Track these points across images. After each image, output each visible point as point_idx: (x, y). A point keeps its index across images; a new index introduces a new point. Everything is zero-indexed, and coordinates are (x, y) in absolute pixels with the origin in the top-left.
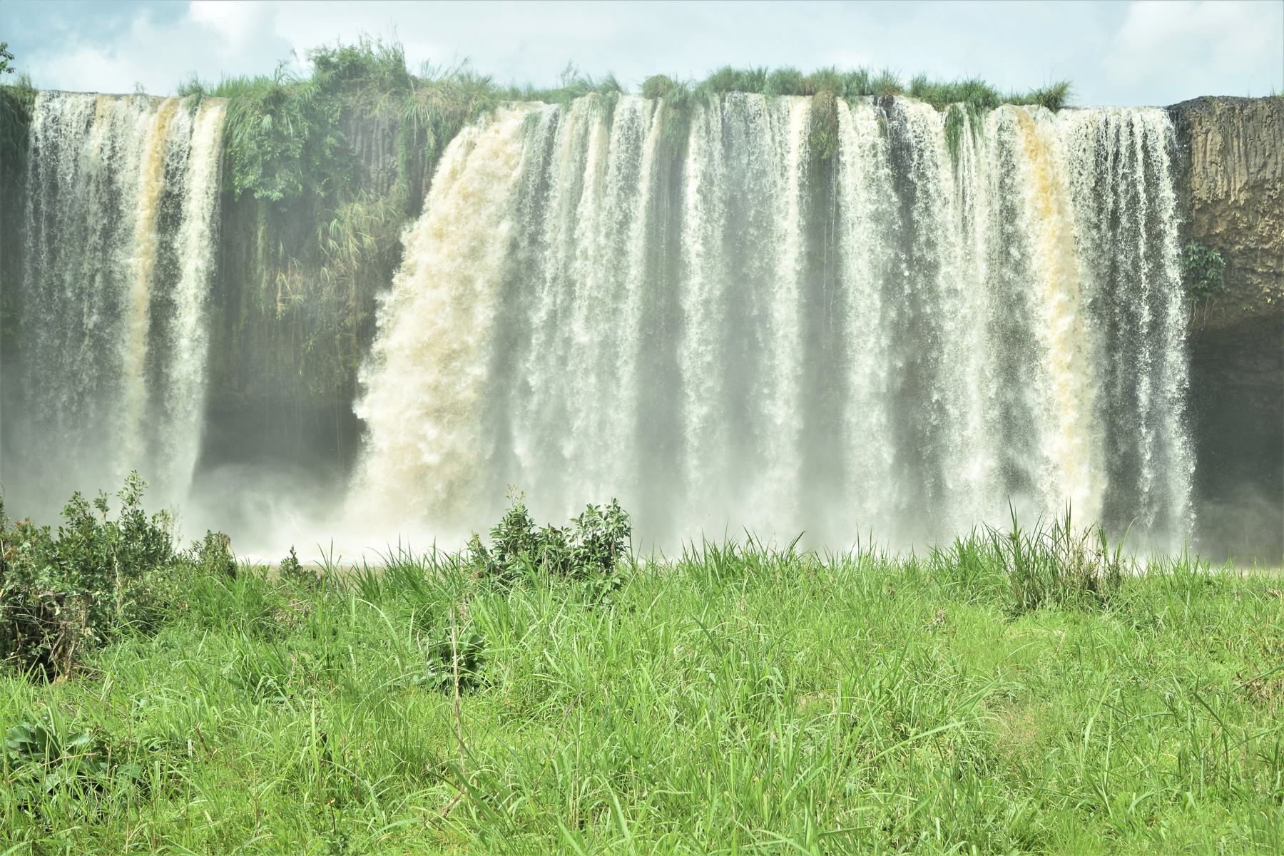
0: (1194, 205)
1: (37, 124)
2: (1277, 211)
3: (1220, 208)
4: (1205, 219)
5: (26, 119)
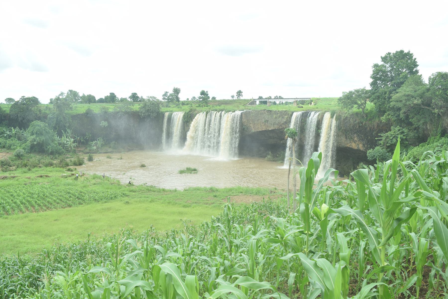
5: (172, 115)
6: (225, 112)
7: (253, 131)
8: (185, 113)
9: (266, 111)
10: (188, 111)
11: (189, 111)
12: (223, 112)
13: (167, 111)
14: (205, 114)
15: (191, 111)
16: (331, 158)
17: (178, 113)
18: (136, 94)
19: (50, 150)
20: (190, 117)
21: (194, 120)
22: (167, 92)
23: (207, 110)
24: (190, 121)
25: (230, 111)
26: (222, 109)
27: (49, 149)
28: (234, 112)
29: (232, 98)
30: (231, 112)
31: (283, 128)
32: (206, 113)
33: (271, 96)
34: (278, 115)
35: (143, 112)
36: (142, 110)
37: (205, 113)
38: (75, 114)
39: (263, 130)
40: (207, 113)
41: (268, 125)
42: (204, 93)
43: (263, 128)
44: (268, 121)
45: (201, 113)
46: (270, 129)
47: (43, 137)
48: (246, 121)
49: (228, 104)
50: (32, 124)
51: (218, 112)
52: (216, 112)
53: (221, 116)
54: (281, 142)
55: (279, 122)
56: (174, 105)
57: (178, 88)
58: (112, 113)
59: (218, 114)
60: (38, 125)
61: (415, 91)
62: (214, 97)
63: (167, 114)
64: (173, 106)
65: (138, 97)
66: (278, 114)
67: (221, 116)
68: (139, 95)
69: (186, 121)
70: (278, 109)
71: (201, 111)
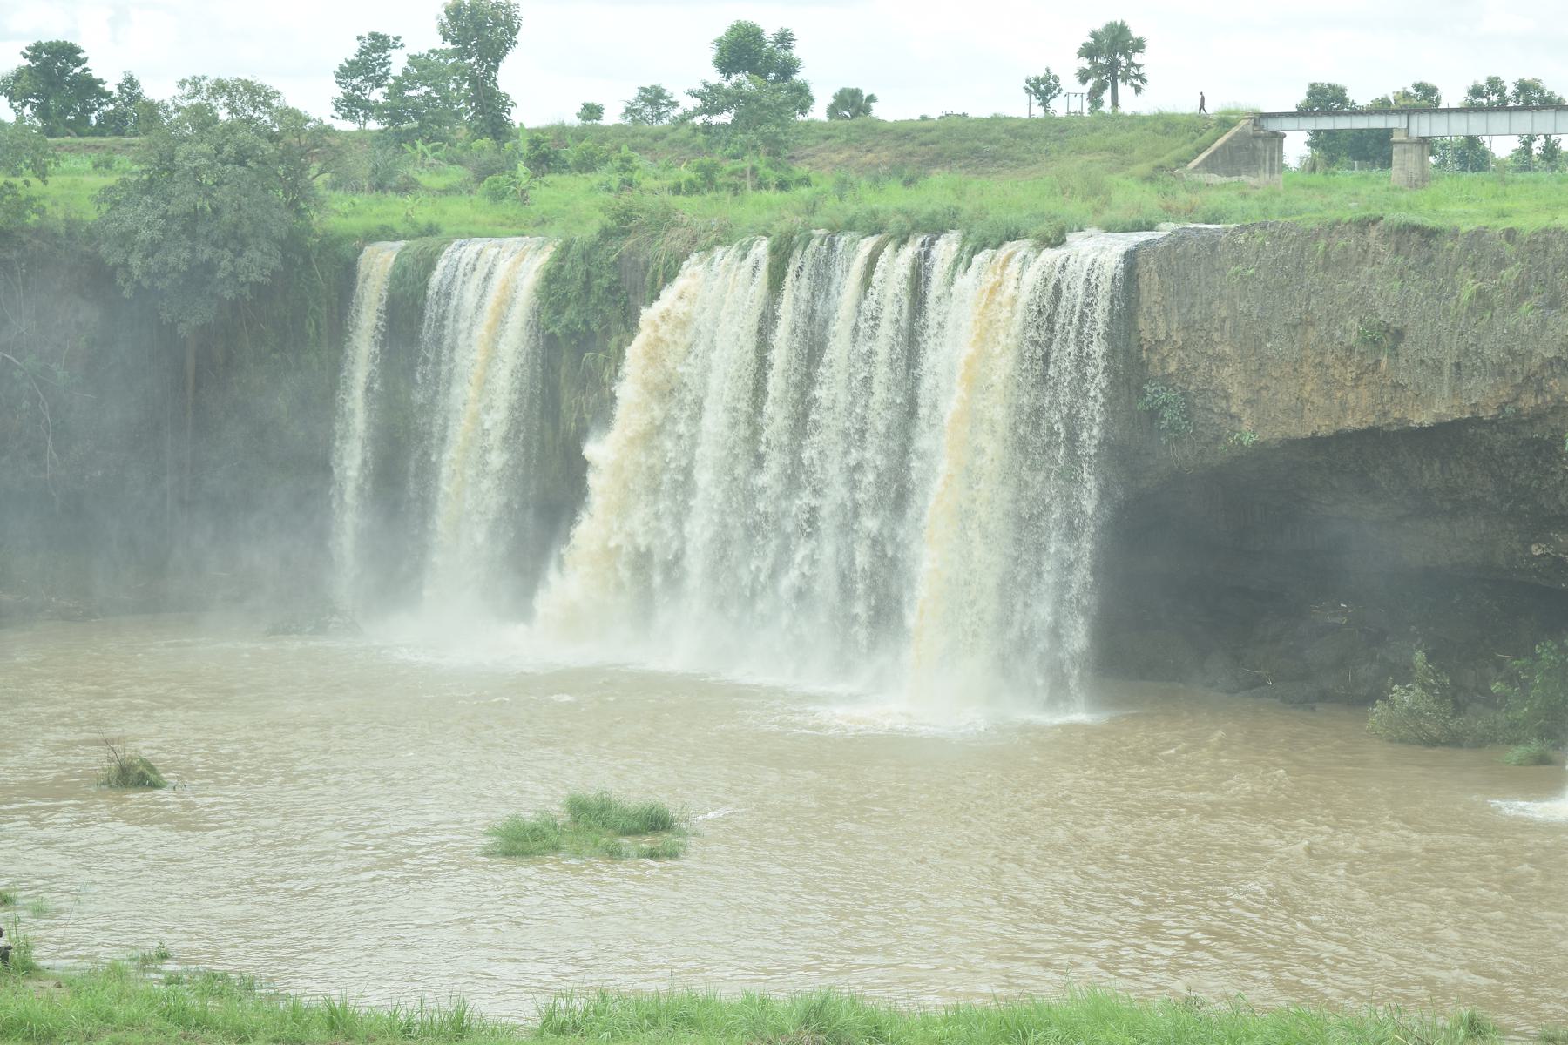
0: (1142, 346)
1: (436, 278)
2: (1210, 352)
3: (1165, 349)
4: (1155, 358)
5: (430, 266)
6: (965, 239)
7: (1248, 439)
8: (566, 248)
9: (1385, 238)
11: (606, 234)
12: (946, 248)
13: (385, 233)
15: (626, 233)
18: (69, 52)
20: (613, 289)
23: (781, 227)
24: (607, 333)
25: (1013, 235)
26: (932, 218)
29: (1035, 102)
30: (1021, 247)
31: (1554, 411)
32: (774, 251)
33: (1430, 81)
34: (1510, 274)
39: (1351, 423)
41: (1403, 377)
42: (758, 54)
43: (1344, 407)
44: (1399, 335)
46: (1423, 418)
48: (1178, 337)
49: (995, 159)
51: (889, 250)
52: (867, 245)
53: (918, 280)
54: (1536, 550)
55: (1517, 346)
56: (456, 175)
59: (897, 265)
62: (856, 93)
63: (378, 263)
64: (439, 182)
65: (89, 87)
66: (1501, 263)
67: (918, 280)
68: (106, 68)
71: (725, 235)
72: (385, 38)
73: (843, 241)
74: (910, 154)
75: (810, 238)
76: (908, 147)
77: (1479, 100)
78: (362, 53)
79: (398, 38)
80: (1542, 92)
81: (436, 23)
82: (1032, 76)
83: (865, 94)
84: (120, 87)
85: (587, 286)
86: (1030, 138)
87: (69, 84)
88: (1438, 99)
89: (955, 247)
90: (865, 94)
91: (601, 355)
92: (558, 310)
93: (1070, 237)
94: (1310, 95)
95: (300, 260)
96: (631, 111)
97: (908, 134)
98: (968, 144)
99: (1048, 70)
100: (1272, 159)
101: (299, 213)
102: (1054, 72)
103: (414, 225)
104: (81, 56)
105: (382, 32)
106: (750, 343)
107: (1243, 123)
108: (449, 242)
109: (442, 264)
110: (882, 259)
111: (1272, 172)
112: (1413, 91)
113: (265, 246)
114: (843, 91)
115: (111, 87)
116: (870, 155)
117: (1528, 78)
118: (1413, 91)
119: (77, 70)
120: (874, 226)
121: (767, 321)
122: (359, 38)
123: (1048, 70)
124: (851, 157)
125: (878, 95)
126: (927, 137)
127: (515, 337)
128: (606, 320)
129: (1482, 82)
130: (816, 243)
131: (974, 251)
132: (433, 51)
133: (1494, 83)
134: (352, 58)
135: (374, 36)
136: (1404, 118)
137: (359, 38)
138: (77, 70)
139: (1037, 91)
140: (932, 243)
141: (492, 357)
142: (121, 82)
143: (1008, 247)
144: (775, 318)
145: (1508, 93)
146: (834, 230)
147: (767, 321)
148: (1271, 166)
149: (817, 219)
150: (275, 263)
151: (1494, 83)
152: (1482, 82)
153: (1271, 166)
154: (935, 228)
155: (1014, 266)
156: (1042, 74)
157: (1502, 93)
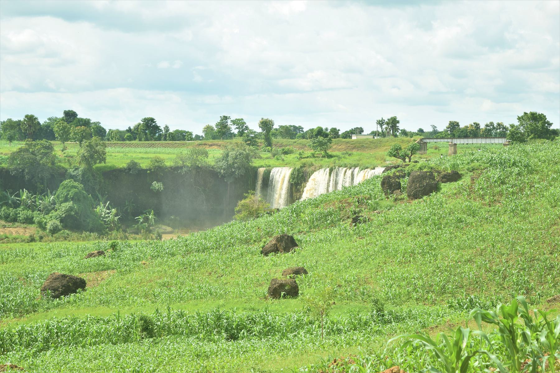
1: (271, 174)
5: (270, 172)
6: (360, 168)
8: (295, 169)
10: (298, 167)
11: (301, 167)
12: (357, 169)
13: (262, 166)
14: (328, 171)
15: (304, 167)
16: (381, 185)
17: (280, 169)
18: (152, 120)
19: (91, 225)
20: (302, 176)
21: (310, 180)
22: (226, 118)
23: (331, 166)
24: (301, 183)
25: (367, 168)
26: (355, 165)
27: (89, 223)
28: (374, 169)
29: (379, 126)
30: (369, 170)
32: (330, 170)
33: (478, 122)
35: (224, 167)
36: (221, 164)
37: (328, 170)
38: (109, 170)
40: (331, 171)
42: (322, 132)
45: (322, 171)
47: (81, 204)
49: (367, 147)
50: (63, 185)
51: (348, 169)
52: (345, 169)
53: (353, 175)
56: (269, 155)
57: (270, 119)
58: (170, 169)
59: (349, 172)
60: (75, 186)
61: (26, 228)
62: (335, 129)
63: (262, 170)
64: (265, 156)
65: (157, 128)
67: (353, 175)
68: (161, 123)
69: (295, 183)
70: (22, 245)
71: (321, 167)
72: (227, 117)
73: (340, 169)
74: (349, 146)
75: (335, 168)
76: (348, 145)
77: (488, 127)
78: (221, 120)
79: (230, 117)
80: (503, 126)
81: (258, 125)
82: (378, 120)
83: (337, 129)
84: (164, 128)
85: (298, 176)
86: (374, 143)
87: (152, 127)
88: (480, 126)
89: (358, 169)
90: (337, 129)
91: (300, 187)
92: (293, 179)
93: (375, 168)
94: (449, 124)
95: (248, 171)
96: (359, 184)
97: (348, 142)
98: (361, 144)
99: (382, 118)
100: (425, 148)
101: (248, 163)
102: (384, 119)
103: (266, 165)
104: (155, 121)
105: (226, 116)
106: (326, 185)
107: (418, 140)
108: (273, 168)
109: (272, 172)
110: (347, 171)
111: (424, 150)
112: (473, 124)
113: (243, 169)
114: (332, 128)
115: (162, 128)
116: (340, 147)
117: (500, 122)
118: (473, 124)
119: (154, 124)
120: (346, 166)
121: (329, 181)
122: (221, 117)
123: (382, 118)
124: (336, 147)
125: (340, 129)
126: (353, 143)
127: (286, 185)
128: (301, 181)
129: (488, 123)
130: (336, 169)
131: (361, 170)
132: (237, 119)
133: (492, 124)
134: (219, 121)
135: (224, 117)
136: (451, 140)
137: (221, 117)
138: (154, 124)
139: (379, 124)
140: (355, 169)
141: (281, 189)
142: (164, 127)
143: (366, 170)
144: (330, 181)
145: (495, 126)
146: (339, 167)
147: (329, 181)
148: (424, 149)
149: (336, 165)
150: (244, 172)
151: (492, 124)
152: (488, 123)
153: (424, 149)
154: (356, 166)
155: (367, 172)
156: (381, 119)
157: (493, 126)
